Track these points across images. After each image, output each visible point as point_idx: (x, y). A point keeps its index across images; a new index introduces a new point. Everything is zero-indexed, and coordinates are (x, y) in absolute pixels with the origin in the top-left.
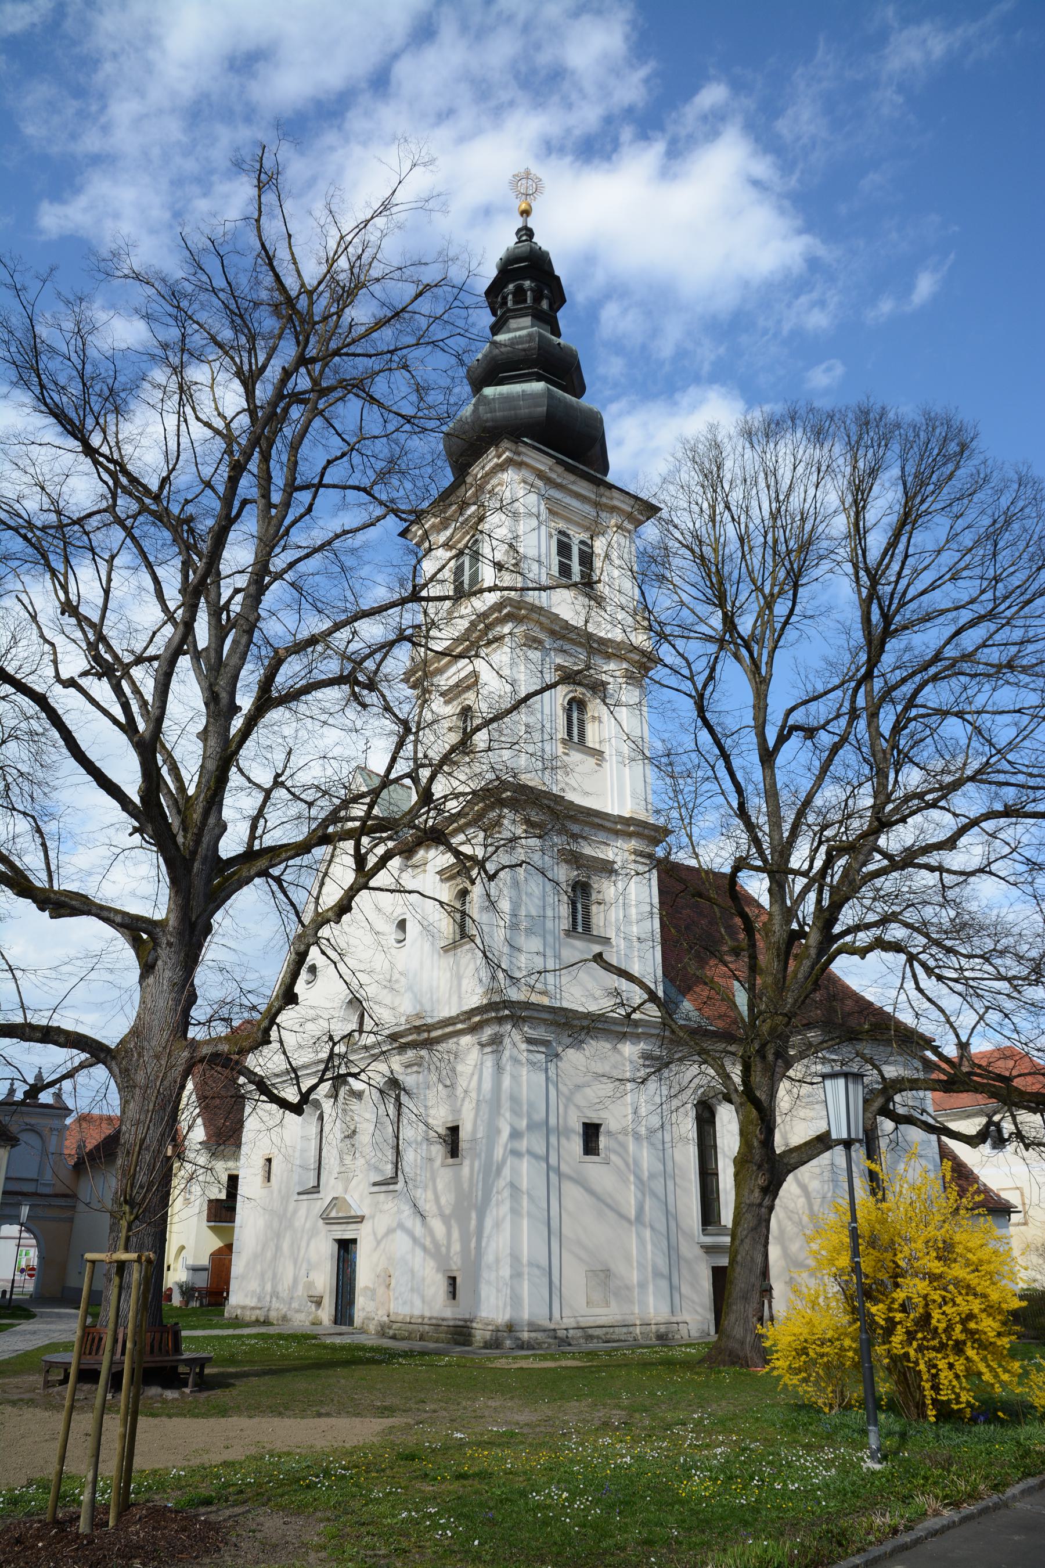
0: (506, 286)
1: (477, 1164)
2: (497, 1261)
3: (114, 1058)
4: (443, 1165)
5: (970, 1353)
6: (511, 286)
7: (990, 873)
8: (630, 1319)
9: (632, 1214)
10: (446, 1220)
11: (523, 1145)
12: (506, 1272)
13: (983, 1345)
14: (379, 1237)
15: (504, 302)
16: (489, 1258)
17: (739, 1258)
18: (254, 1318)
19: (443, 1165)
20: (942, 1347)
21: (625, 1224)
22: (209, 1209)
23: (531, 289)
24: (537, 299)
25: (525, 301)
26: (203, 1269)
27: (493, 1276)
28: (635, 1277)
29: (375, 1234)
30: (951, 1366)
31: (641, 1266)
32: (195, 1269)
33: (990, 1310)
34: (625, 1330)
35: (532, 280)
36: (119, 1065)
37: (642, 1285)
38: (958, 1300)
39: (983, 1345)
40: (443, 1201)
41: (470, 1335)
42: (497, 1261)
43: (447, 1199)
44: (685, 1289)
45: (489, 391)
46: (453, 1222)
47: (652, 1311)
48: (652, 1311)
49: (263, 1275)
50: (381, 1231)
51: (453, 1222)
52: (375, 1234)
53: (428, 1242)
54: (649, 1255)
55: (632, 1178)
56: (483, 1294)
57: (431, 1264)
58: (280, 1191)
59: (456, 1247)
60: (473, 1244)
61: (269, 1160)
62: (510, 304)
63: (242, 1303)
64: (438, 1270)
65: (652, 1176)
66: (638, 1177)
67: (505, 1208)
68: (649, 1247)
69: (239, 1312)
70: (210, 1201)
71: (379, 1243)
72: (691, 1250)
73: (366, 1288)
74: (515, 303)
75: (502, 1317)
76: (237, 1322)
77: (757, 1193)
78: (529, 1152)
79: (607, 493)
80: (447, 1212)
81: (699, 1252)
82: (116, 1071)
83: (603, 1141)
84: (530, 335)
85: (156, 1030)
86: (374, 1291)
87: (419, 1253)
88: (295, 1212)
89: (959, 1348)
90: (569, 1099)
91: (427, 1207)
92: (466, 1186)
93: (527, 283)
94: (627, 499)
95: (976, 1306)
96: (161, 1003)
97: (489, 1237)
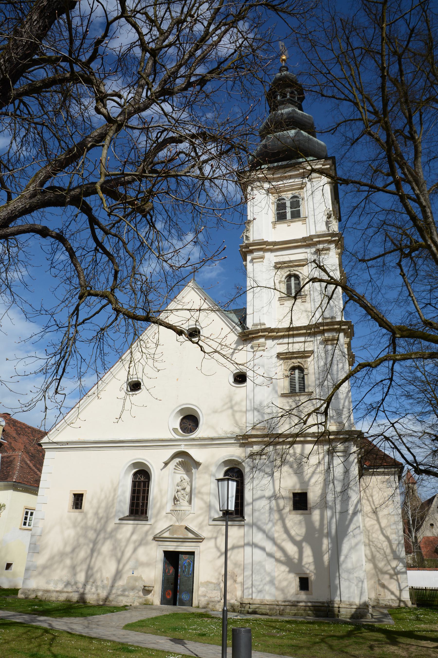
10: (298, 544)
46: (304, 544)
51: (304, 544)
57: (284, 568)
69: (40, 594)
97: (346, 557)
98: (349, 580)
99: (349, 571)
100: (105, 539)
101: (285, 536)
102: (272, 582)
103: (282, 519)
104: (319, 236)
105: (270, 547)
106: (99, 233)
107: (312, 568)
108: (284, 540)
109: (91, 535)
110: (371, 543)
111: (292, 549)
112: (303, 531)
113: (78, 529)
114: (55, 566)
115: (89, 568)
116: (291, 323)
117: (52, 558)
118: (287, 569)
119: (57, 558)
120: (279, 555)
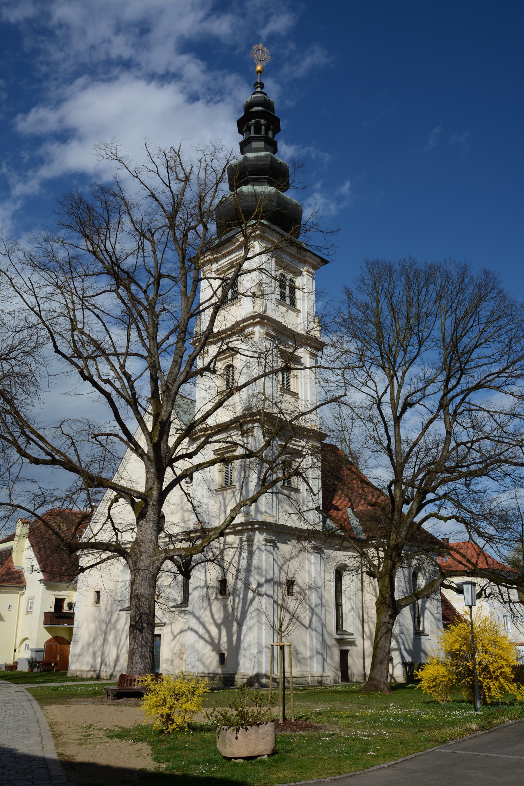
0: (250, 121)
1: (237, 600)
2: (250, 645)
3: (130, 556)
4: (216, 598)
5: (502, 680)
6: (253, 121)
7: (488, 476)
8: (306, 674)
9: (307, 624)
10: (218, 626)
11: (263, 590)
12: (255, 651)
13: (506, 678)
14: (175, 634)
15: (248, 129)
16: (244, 644)
17: (379, 645)
18: (89, 676)
19: (216, 598)
20: (491, 678)
21: (304, 628)
22: (45, 617)
23: (265, 125)
24: (267, 132)
25: (260, 133)
26: (41, 651)
27: (247, 653)
28: (308, 654)
29: (172, 633)
30: (494, 685)
31: (311, 649)
32: (37, 651)
33: (509, 665)
34: (303, 679)
35: (265, 120)
36: (132, 559)
37: (311, 658)
38: (498, 661)
39: (506, 678)
40: (216, 617)
41: (234, 681)
42: (250, 645)
43: (219, 616)
44: (329, 661)
45: (246, 189)
46: (222, 627)
47: (315, 670)
48: (315, 670)
49: (94, 654)
50: (177, 631)
51: (222, 627)
52: (172, 633)
53: (207, 637)
54: (315, 644)
55: (307, 607)
56: (241, 662)
57: (209, 647)
58: (106, 609)
59: (224, 639)
60: (235, 638)
61: (98, 593)
62: (252, 133)
63: (79, 669)
64: (213, 650)
65: (316, 606)
66: (310, 607)
67: (255, 620)
68: (315, 640)
69: (78, 673)
70: (45, 613)
71: (175, 637)
72: (330, 642)
73: (167, 660)
74: (255, 132)
75: (251, 673)
76: (76, 679)
77: (387, 618)
78: (266, 594)
79: (304, 253)
80: (219, 621)
81: (334, 642)
82: (130, 562)
83: (295, 589)
84: (266, 156)
85: (148, 543)
86: (172, 662)
87: (202, 642)
88: (117, 620)
89: (497, 678)
90: (281, 568)
91: (206, 619)
92: (230, 610)
93: (262, 121)
94: (314, 257)
95: (504, 663)
96: (149, 532)
97: (245, 635)
98: (245, 656)
99: (245, 649)
100: (111, 630)
101: (211, 620)
102: (200, 660)
103: (210, 605)
104: (244, 321)
105: (201, 631)
106: (105, 216)
107: (226, 647)
108: (210, 624)
109: (104, 627)
110: (370, 619)
111: (214, 631)
112: (222, 615)
113: (97, 623)
114: (85, 654)
115: (103, 654)
116: (180, 486)
117: (83, 648)
118: (212, 648)
119: (86, 647)
120: (207, 637)
